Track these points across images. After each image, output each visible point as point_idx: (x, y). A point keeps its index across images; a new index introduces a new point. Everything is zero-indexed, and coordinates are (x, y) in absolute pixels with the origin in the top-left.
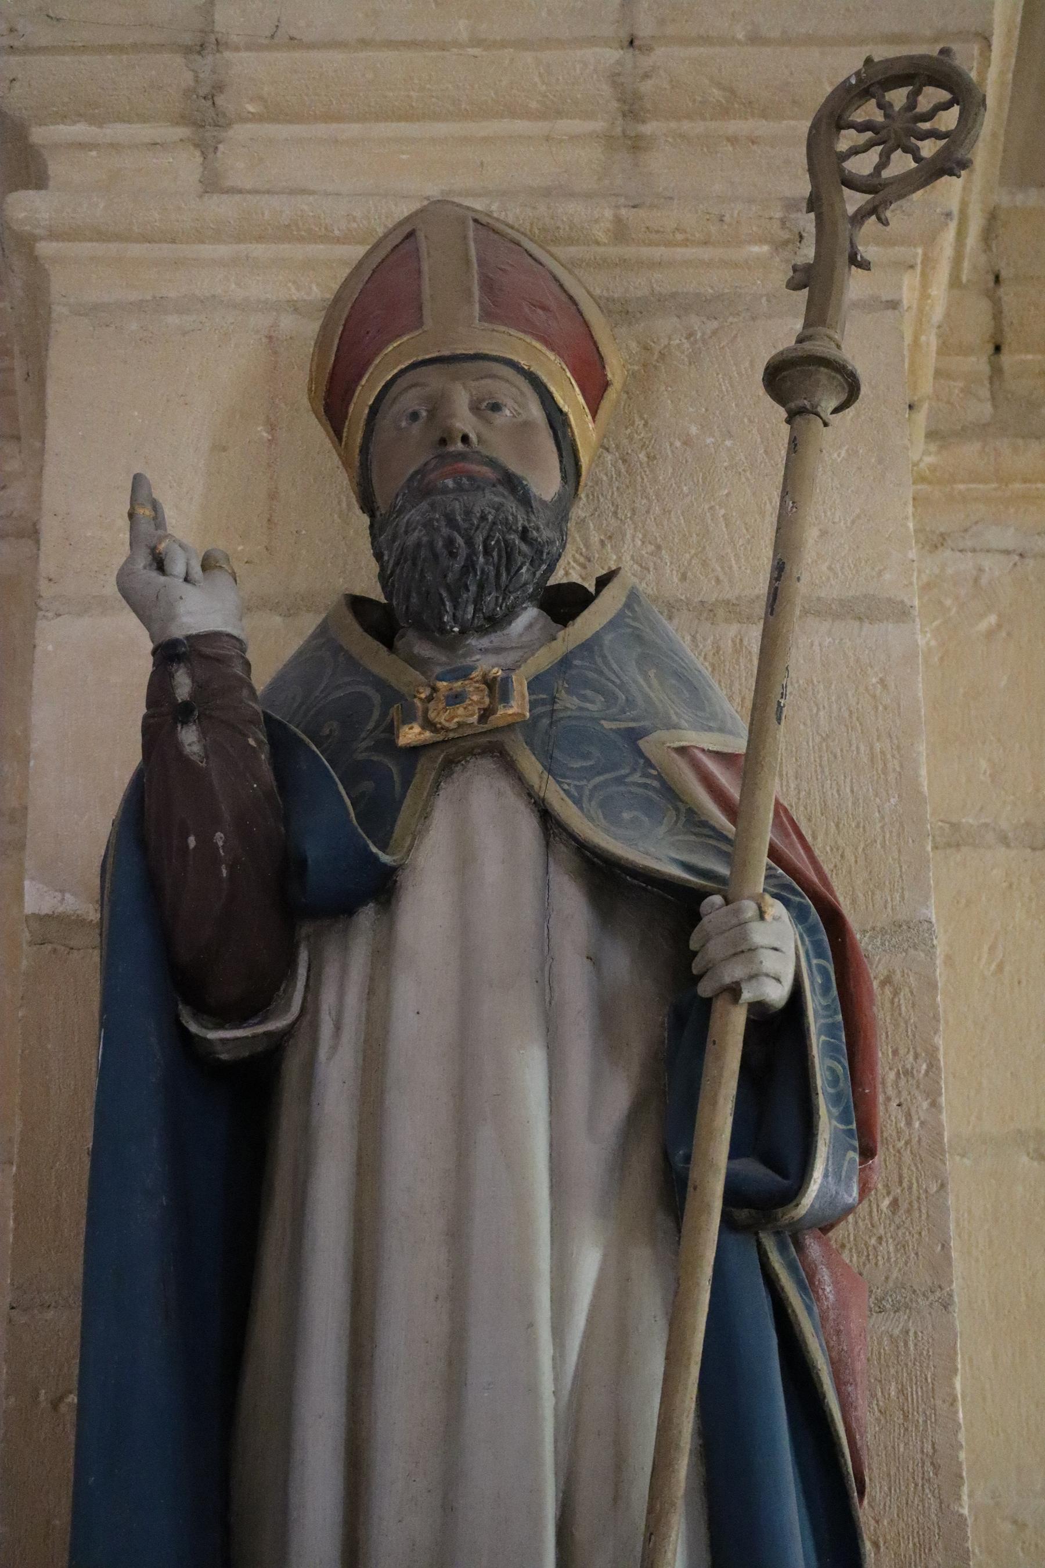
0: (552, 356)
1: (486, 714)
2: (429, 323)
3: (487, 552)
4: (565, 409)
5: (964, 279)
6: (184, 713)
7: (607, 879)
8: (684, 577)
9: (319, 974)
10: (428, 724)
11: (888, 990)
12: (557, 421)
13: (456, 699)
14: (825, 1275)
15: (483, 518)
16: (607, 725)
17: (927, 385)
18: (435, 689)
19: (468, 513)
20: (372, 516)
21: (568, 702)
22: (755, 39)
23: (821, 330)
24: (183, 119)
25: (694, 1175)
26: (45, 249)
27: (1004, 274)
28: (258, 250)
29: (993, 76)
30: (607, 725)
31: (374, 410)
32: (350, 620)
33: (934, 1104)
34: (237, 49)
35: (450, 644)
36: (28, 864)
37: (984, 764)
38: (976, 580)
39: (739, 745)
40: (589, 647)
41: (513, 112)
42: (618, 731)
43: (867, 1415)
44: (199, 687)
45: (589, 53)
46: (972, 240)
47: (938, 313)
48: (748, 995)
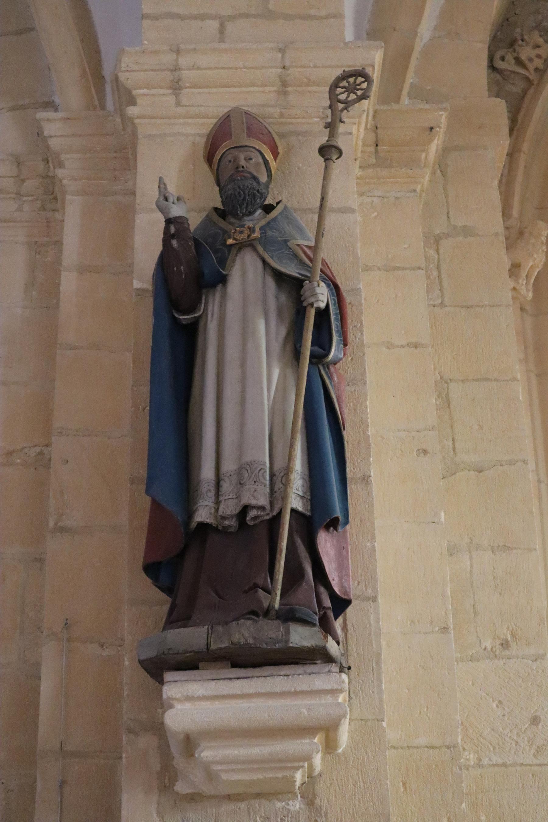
0: (264, 146)
1: (249, 236)
2: (233, 138)
3: (249, 196)
4: (268, 159)
5: (368, 127)
6: (173, 236)
7: (280, 278)
8: (298, 203)
9: (208, 302)
10: (234, 239)
11: (350, 306)
12: (266, 162)
13: (241, 232)
14: (335, 375)
15: (248, 187)
16: (279, 238)
17: (359, 154)
18: (236, 230)
19: (244, 185)
20: (220, 187)
21: (270, 233)
22: (315, 67)
23: (333, 138)
24: (171, 88)
25: (302, 351)
26: (137, 121)
27: (378, 126)
28: (190, 121)
29: (376, 76)
30: (279, 238)
31: (220, 160)
32: (215, 213)
33: (362, 334)
34: (184, 70)
35: (240, 219)
36: (134, 276)
37: (374, 250)
38: (372, 204)
39: (312, 244)
40: (275, 219)
41: (254, 85)
42: (282, 240)
43: (346, 410)
44: (177, 230)
45: (273, 70)
46: (370, 118)
47: (362, 136)
48: (315, 305)
